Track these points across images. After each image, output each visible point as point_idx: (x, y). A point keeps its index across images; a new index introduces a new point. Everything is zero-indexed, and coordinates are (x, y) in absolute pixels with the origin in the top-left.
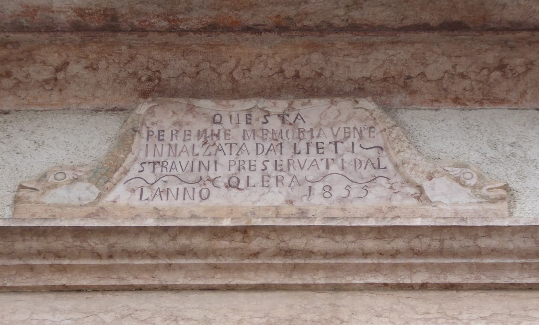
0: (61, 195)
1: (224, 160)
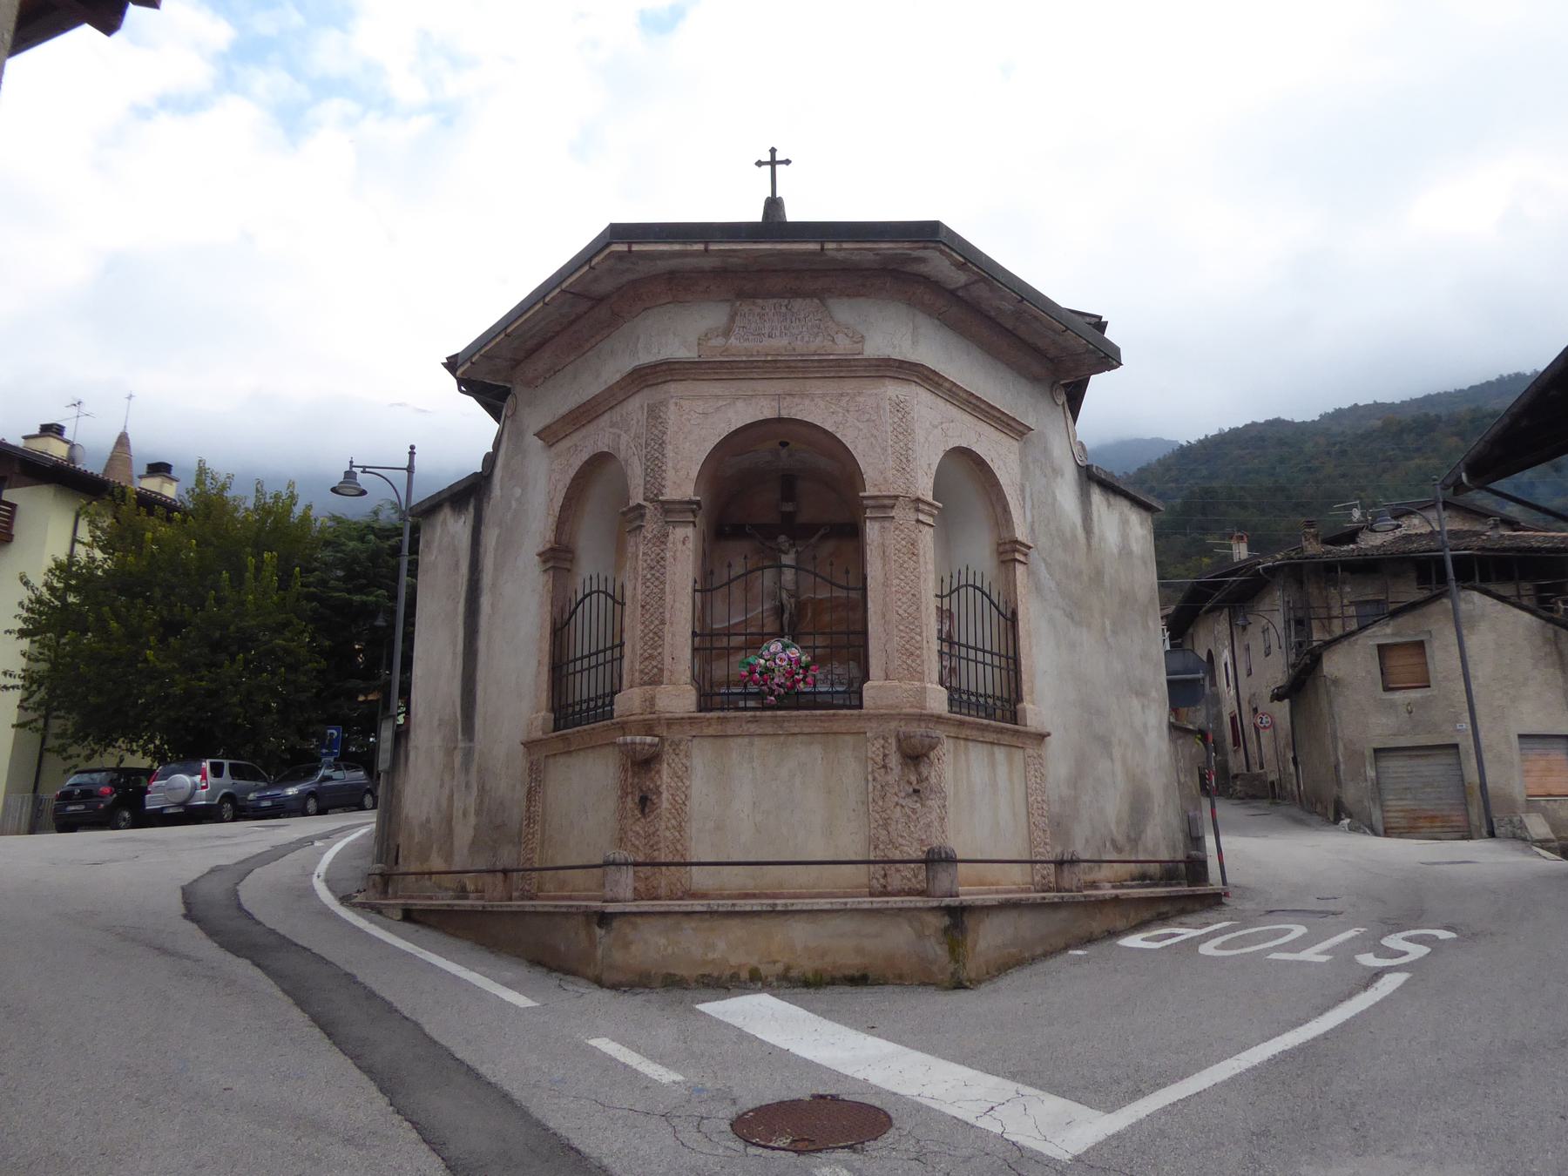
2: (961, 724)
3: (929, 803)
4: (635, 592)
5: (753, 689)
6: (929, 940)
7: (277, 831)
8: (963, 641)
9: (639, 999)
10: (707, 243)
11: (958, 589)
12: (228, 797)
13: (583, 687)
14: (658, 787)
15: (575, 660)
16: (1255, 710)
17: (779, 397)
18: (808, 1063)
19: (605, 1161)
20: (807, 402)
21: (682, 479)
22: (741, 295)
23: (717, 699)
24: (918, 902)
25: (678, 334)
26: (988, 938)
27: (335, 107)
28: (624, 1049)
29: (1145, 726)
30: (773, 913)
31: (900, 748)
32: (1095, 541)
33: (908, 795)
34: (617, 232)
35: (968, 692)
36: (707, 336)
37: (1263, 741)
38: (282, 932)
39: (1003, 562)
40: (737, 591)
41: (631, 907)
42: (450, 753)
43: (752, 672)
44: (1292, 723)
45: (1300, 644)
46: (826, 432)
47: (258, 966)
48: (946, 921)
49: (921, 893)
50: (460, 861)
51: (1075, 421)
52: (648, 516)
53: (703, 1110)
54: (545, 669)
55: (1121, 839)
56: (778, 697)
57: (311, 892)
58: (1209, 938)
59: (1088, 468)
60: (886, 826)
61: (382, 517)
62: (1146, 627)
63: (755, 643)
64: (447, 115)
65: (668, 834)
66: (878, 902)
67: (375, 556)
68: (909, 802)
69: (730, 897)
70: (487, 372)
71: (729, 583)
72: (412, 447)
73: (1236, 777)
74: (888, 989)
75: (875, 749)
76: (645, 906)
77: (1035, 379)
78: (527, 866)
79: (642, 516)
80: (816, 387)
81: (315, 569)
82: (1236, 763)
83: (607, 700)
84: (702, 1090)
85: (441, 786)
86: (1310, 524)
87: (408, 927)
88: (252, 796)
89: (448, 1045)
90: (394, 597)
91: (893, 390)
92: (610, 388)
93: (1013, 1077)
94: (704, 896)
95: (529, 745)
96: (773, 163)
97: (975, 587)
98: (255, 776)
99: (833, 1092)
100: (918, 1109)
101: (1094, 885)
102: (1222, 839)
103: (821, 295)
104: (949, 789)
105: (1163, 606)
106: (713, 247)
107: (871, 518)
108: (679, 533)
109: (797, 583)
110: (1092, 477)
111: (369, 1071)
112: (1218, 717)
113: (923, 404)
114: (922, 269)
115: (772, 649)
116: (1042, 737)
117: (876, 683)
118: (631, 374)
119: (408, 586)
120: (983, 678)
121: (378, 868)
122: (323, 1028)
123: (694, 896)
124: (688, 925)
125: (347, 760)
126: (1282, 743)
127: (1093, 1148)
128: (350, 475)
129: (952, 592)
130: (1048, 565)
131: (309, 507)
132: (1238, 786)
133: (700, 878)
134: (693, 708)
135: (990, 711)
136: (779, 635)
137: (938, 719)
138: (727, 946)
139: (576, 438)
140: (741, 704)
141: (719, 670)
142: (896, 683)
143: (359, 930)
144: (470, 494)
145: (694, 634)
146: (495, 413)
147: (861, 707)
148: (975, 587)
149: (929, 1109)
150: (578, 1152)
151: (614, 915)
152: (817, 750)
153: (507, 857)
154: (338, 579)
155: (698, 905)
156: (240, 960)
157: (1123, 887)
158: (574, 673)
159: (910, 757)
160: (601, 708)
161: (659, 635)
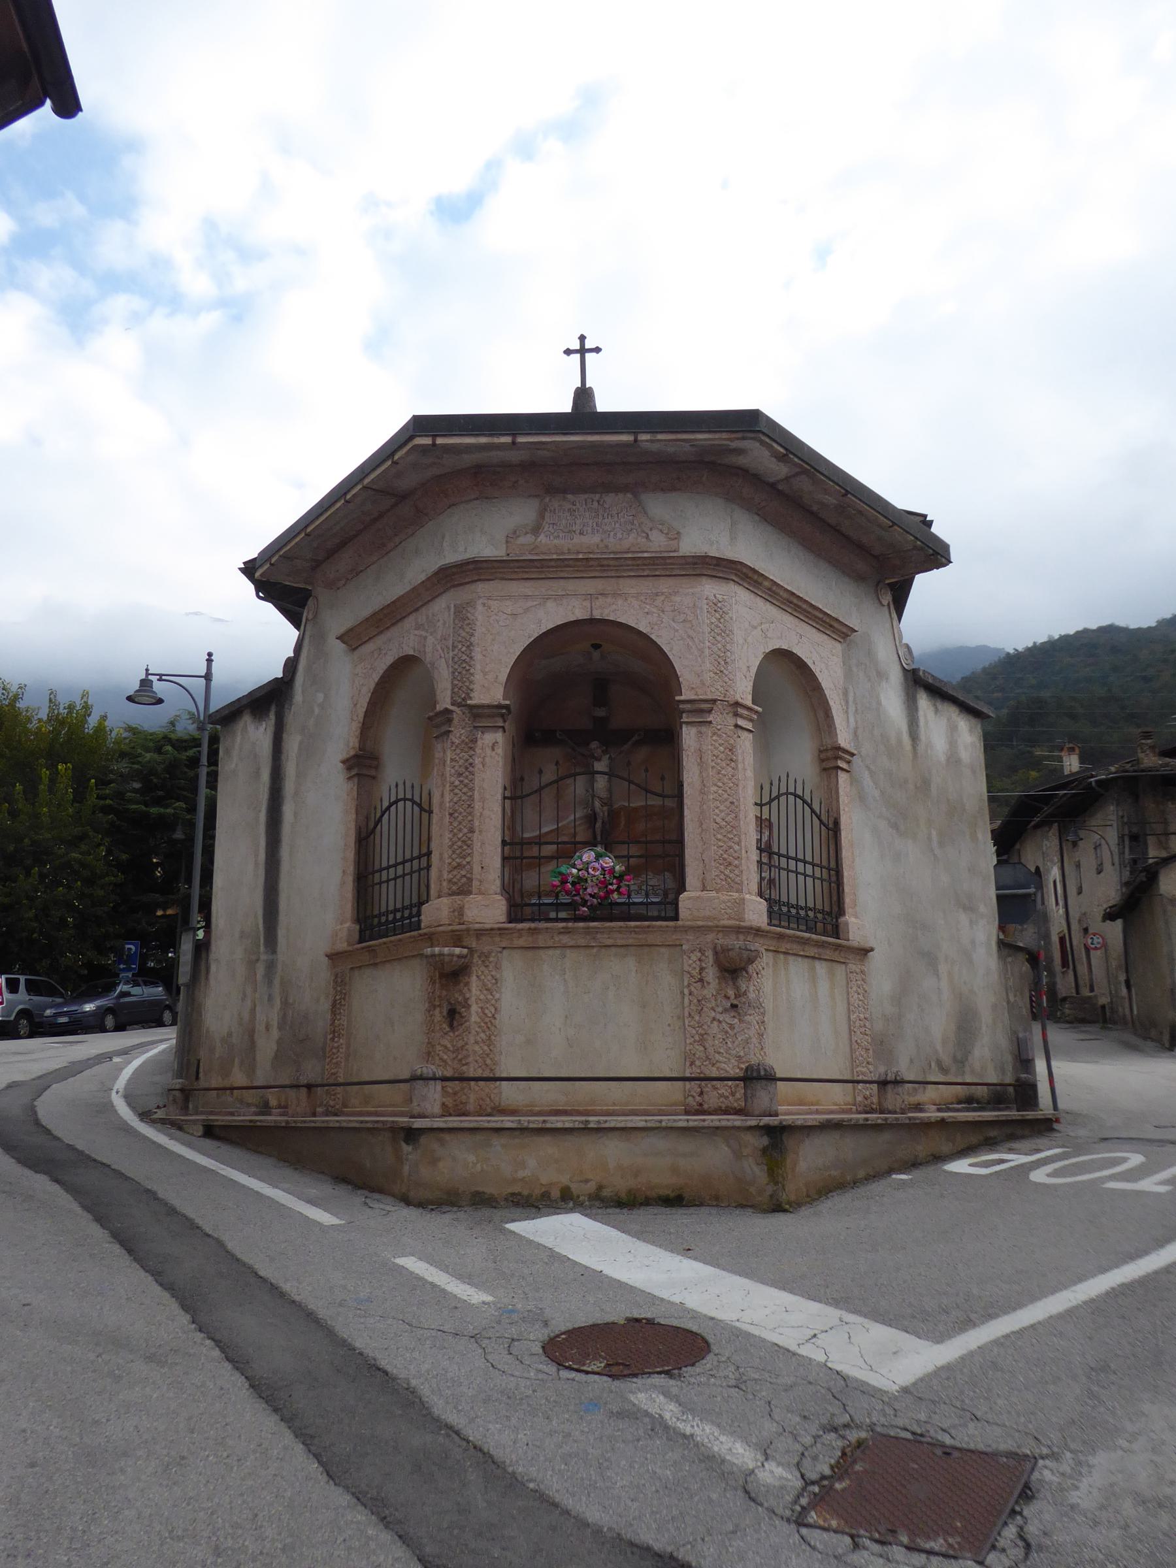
0: (522, 540)
1: (578, 522)
2: (781, 937)
3: (747, 1018)
4: (442, 798)
5: (565, 899)
6: (747, 1161)
7: (75, 1047)
8: (783, 851)
9: (447, 1218)
10: (514, 435)
11: (778, 797)
12: (24, 1013)
13: (389, 897)
14: (466, 1000)
15: (374, 872)
16: (1086, 930)
17: (591, 597)
18: (621, 1285)
19: (414, 1382)
20: (620, 602)
21: (491, 684)
22: (552, 490)
23: (528, 910)
24: (737, 1121)
25: (484, 531)
26: (809, 1159)
27: (121, 304)
28: (432, 1268)
29: (973, 942)
30: (586, 1130)
31: (718, 962)
32: (921, 748)
33: (726, 1010)
34: (420, 425)
35: (788, 905)
36: (515, 534)
37: (1094, 962)
38: (80, 1147)
39: (825, 769)
40: (548, 796)
41: (439, 1123)
42: (251, 964)
43: (564, 881)
44: (1125, 944)
45: (1135, 861)
46: (640, 633)
47: (57, 1181)
48: (765, 1141)
49: (738, 1112)
50: (262, 1076)
51: (900, 620)
52: (455, 721)
53: (513, 1331)
54: (350, 879)
55: (947, 1060)
56: (591, 907)
57: (109, 1107)
58: (1041, 1166)
59: (915, 672)
60: (702, 1041)
61: (179, 728)
62: (974, 838)
63: (567, 853)
64: (238, 311)
65: (477, 1048)
66: (695, 1120)
67: (172, 767)
68: (727, 1017)
69: (539, 1114)
70: (286, 575)
71: (541, 788)
72: (210, 654)
73: (1064, 999)
74: (704, 1210)
75: (690, 962)
76: (454, 1121)
77: (859, 578)
78: (331, 1081)
79: (450, 721)
80: (630, 586)
81: (110, 782)
82: (1065, 985)
83: (415, 910)
84: (512, 1311)
85: (243, 1000)
86: (1147, 735)
87: (208, 1143)
88: (48, 1012)
89: (251, 1262)
90: (193, 809)
91: (710, 589)
92: (414, 589)
93: (836, 1303)
94: (513, 1112)
95: (333, 957)
96: (582, 351)
97: (796, 796)
98: (51, 992)
99: (649, 1315)
100: (737, 1335)
101: (918, 1107)
102: (1054, 1063)
103: (634, 489)
104: (768, 1005)
105: (992, 819)
106: (521, 439)
107: (687, 723)
108: (489, 738)
109: (610, 790)
110: (920, 682)
111: (169, 1287)
112: (1047, 937)
113: (742, 603)
114: (742, 461)
115: (585, 858)
116: (865, 952)
117: (693, 894)
118: (436, 573)
119: (207, 797)
120: (803, 890)
121: (178, 1083)
122: (122, 1243)
123: (503, 1112)
124: (497, 1142)
125: (145, 976)
126: (1114, 964)
127: (922, 1380)
128: (145, 683)
129: (771, 800)
130: (872, 774)
131: (104, 718)
132: (1067, 1009)
133: (510, 1093)
134: (503, 918)
135: (811, 924)
136: (592, 844)
137: (757, 932)
138: (538, 1164)
139: (380, 641)
140: (553, 915)
141: (530, 880)
142: (713, 894)
143: (160, 1146)
144: (270, 699)
145: (504, 843)
146: (295, 619)
147: (676, 918)
148: (796, 796)
149: (749, 1335)
150: (386, 1373)
151: (422, 1131)
152: (631, 962)
153: (311, 1071)
154: (135, 791)
155: (508, 1122)
156: (38, 1176)
157: (949, 1110)
158: (380, 883)
159: (726, 970)
160: (407, 919)
161: (467, 843)
